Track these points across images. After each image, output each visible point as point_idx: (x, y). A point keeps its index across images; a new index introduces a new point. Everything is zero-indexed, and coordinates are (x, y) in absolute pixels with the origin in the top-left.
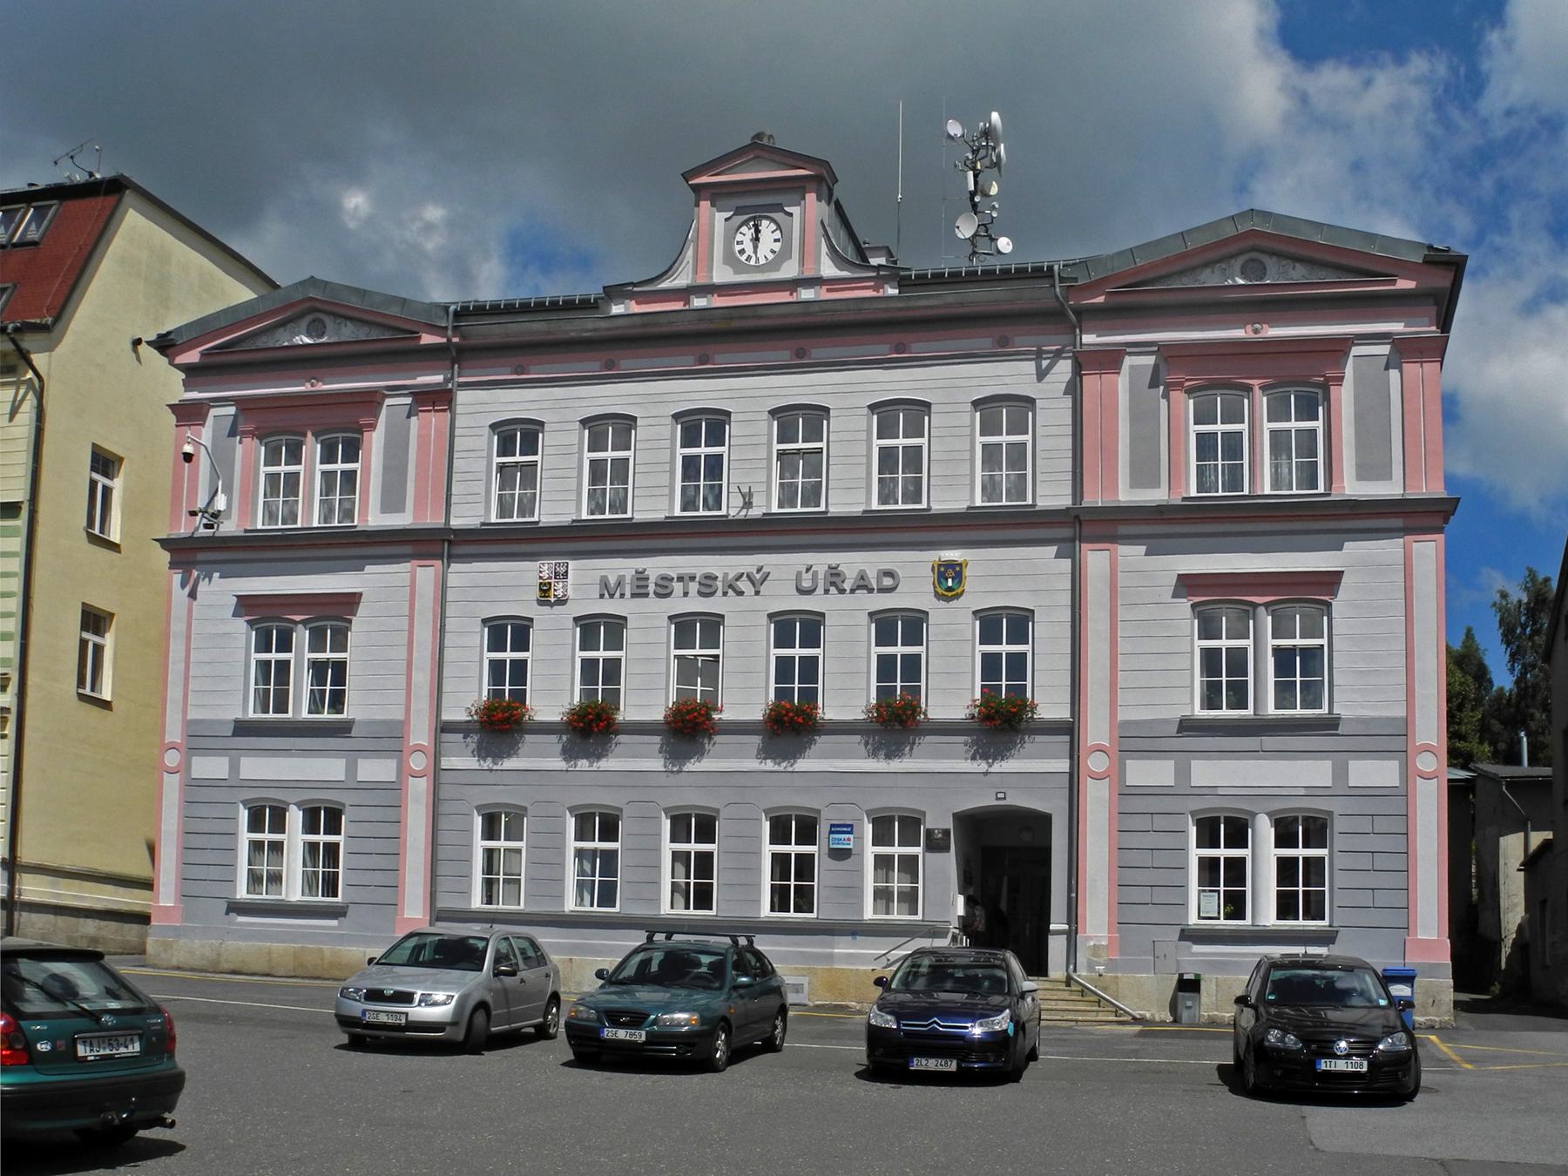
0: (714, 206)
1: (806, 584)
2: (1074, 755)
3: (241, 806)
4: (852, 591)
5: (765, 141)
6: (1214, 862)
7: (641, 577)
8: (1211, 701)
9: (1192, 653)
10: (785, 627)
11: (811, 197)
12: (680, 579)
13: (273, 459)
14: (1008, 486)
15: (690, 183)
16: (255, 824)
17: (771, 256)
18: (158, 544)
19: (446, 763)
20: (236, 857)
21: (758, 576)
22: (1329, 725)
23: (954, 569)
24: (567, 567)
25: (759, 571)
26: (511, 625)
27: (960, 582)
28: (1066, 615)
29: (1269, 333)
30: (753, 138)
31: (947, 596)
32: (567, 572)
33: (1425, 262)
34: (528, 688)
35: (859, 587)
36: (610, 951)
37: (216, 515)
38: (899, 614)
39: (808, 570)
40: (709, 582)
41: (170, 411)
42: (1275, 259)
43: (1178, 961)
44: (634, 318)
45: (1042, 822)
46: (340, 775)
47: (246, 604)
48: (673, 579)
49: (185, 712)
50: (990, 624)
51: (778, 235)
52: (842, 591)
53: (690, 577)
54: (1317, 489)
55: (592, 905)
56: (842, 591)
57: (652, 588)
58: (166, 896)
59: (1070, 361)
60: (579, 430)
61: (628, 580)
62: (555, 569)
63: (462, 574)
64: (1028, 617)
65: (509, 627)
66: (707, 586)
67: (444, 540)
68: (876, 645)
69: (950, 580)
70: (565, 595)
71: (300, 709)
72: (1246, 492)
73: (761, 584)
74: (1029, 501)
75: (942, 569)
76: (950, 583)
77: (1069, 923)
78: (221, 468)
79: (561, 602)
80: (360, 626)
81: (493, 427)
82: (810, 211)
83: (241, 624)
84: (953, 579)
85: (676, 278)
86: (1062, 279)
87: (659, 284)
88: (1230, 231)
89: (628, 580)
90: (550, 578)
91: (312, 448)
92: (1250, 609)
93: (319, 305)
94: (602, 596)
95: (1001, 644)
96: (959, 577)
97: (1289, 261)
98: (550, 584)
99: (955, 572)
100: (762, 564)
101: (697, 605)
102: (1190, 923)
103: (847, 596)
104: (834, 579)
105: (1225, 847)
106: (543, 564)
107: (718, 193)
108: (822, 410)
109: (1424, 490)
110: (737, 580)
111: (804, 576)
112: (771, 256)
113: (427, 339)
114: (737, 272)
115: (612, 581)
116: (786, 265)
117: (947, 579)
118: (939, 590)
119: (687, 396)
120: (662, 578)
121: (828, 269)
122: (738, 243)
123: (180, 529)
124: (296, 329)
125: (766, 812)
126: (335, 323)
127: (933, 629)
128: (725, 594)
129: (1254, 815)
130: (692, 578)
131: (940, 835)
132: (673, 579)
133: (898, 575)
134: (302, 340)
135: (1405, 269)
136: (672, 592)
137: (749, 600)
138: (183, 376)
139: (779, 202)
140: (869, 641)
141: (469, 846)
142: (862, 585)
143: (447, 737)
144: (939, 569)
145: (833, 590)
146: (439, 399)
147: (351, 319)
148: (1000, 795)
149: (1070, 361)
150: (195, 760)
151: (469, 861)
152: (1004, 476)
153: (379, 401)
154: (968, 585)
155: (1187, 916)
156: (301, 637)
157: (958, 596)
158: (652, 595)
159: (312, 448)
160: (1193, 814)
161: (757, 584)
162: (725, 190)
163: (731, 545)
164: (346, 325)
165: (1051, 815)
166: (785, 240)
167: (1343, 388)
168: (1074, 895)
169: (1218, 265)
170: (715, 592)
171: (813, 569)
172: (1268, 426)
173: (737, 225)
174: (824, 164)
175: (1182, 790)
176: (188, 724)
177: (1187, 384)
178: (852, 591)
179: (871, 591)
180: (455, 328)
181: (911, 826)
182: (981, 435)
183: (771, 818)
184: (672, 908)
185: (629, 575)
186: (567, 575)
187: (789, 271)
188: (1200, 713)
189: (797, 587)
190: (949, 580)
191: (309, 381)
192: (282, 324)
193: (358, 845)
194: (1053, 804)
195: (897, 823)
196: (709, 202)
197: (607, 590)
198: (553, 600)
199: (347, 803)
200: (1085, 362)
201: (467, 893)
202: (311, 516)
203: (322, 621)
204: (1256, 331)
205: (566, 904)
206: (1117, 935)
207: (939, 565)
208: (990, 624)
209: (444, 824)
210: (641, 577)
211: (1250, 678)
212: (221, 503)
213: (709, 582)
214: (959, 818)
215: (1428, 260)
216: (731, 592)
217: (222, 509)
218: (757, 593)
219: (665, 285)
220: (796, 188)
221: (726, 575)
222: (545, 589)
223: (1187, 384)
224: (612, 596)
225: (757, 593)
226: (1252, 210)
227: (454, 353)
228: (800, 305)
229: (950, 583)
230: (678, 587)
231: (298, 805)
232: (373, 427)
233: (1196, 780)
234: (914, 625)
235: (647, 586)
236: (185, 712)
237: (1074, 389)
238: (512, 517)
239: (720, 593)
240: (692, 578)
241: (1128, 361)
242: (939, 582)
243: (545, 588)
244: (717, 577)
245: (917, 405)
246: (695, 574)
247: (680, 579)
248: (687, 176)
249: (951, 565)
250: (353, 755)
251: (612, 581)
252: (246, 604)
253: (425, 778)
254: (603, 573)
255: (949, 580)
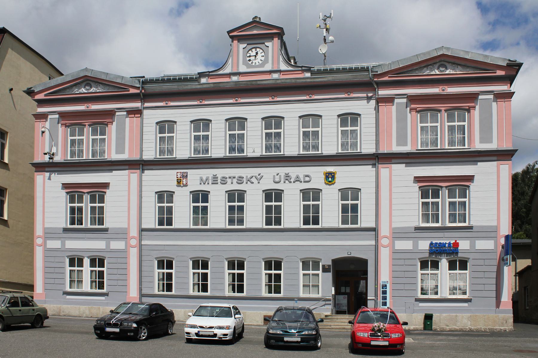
0: (239, 42)
1: (277, 180)
2: (377, 240)
3: (66, 258)
4: (294, 182)
5: (258, 20)
6: (270, 275)
7: (215, 177)
8: (72, 223)
9: (419, 204)
10: (268, 195)
11: (276, 40)
12: (230, 178)
13: (72, 135)
14: (104, 154)
15: (230, 35)
16: (72, 264)
17: (261, 62)
18: (31, 165)
19: (143, 243)
20: (65, 276)
21: (259, 177)
22: (106, 230)
23: (331, 175)
24: (187, 173)
25: (259, 175)
26: (274, 192)
27: (334, 179)
28: (374, 190)
29: (241, 101)
30: (253, 19)
31: (329, 184)
32: (187, 175)
33: (507, 65)
34: (173, 216)
35: (296, 181)
36: (270, 309)
37: (53, 154)
38: (311, 190)
39: (277, 175)
40: (224, 179)
41: (33, 116)
42: (450, 64)
43: (414, 309)
44: (211, 84)
45: (364, 263)
46: (411, 248)
47: (65, 186)
48: (227, 178)
49: (44, 224)
50: (344, 193)
51: (263, 54)
52: (291, 182)
53: (233, 177)
54: (438, 147)
55: (199, 291)
56: (291, 182)
57: (219, 181)
58: (39, 288)
59: (375, 100)
60: (261, 121)
61: (210, 178)
62: (183, 174)
63: (150, 175)
64: (439, 189)
65: (273, 193)
66: (240, 180)
67: (140, 164)
68: (265, 202)
69: (330, 178)
70: (186, 184)
71: (87, 224)
72: (439, 147)
73: (260, 180)
74: (359, 151)
75: (327, 175)
76: (330, 179)
77: (375, 297)
78: (53, 138)
79: (186, 185)
80: (109, 195)
81: (157, 123)
82: (273, 45)
83: (63, 193)
84: (331, 178)
85: (225, 70)
86: (372, 72)
87: (219, 72)
88: (435, 54)
89: (210, 178)
90: (181, 177)
91: (88, 130)
92: (440, 188)
93: (88, 78)
94: (201, 184)
95: (272, 202)
96: (333, 177)
97: (456, 65)
98: (181, 179)
99: (332, 176)
100: (216, 174)
101: (236, 187)
102: (226, 294)
103: (292, 183)
104: (287, 178)
105: (312, 271)
106: (178, 172)
107: (241, 39)
108: (245, 120)
109: (505, 147)
110: (251, 178)
111: (276, 177)
112: (261, 62)
113: (132, 91)
114: (248, 68)
115: (204, 179)
116: (266, 65)
117: (329, 178)
118: (327, 182)
119: (231, 113)
120: (223, 178)
121: (283, 67)
122: (263, 56)
123: (39, 159)
124: (80, 87)
125: (263, 259)
126: (95, 85)
127: (324, 195)
128: (247, 183)
129: (84, 257)
130: (234, 178)
131: (327, 267)
132: (227, 178)
133: (311, 177)
134: (82, 91)
135: (500, 67)
136: (227, 182)
137: (219, 186)
138: (37, 104)
139: (263, 42)
140: (190, 201)
141: (153, 271)
142: (298, 180)
143: (143, 233)
144: (326, 175)
145: (287, 182)
146: (137, 112)
147: (102, 84)
148: (349, 253)
149: (375, 100)
150: (48, 241)
151: (153, 277)
152: (311, 142)
153: (114, 113)
154: (337, 180)
155: (417, 294)
156: (87, 198)
157: (333, 184)
158: (219, 183)
159: (88, 130)
160: (419, 259)
161: (259, 180)
162: (244, 38)
163: (480, 160)
164: (100, 86)
165: (368, 260)
166: (266, 56)
167: (112, 126)
168: (376, 286)
169: (430, 66)
170: (243, 182)
171: (279, 174)
172: (91, 137)
173: (248, 50)
174: (281, 29)
175: (62, 250)
176: (45, 229)
177: (418, 109)
178: (294, 182)
179: (301, 182)
180: (142, 87)
181: (316, 264)
182: (229, 131)
183: (302, 262)
184: (193, 292)
185: (211, 176)
186: (187, 177)
187: (268, 67)
188: (69, 226)
189: (274, 181)
190: (330, 178)
191: (347, 93)
192: (75, 85)
193: (111, 271)
194: (369, 257)
195: (458, 262)
196: (277, 38)
197: (203, 181)
198: (182, 185)
199: (107, 256)
200: (380, 101)
201: (153, 288)
202: (87, 156)
203: (71, 193)
204: (166, 104)
205: (155, 291)
206: (392, 300)
207: (326, 173)
208: (344, 193)
209: (144, 264)
210: (215, 177)
211: (89, 216)
212: (54, 150)
213: (224, 179)
214: (334, 261)
215: (509, 65)
216: (249, 182)
217: (55, 152)
218: (259, 183)
219: (221, 72)
220: (270, 37)
221: (247, 177)
222: (179, 182)
223: (418, 109)
224: (204, 184)
225: (259, 183)
226: (443, 47)
227: (142, 97)
228: (273, 80)
229: (330, 179)
230: (229, 181)
231: (88, 257)
232: (112, 123)
233: (67, 246)
234: (316, 194)
235: (217, 180)
236: (44, 224)
237: (377, 109)
238: (97, 157)
239: (245, 182)
240: (234, 178)
241: (50, 117)
242: (326, 179)
243: (179, 181)
244: (243, 177)
245: (433, 111)
246: (235, 176)
247: (230, 178)
248: (229, 32)
249: (330, 173)
250: (473, 239)
251: (204, 179)
252: (65, 186)
253: (136, 248)
254: (201, 176)
255: (330, 178)
